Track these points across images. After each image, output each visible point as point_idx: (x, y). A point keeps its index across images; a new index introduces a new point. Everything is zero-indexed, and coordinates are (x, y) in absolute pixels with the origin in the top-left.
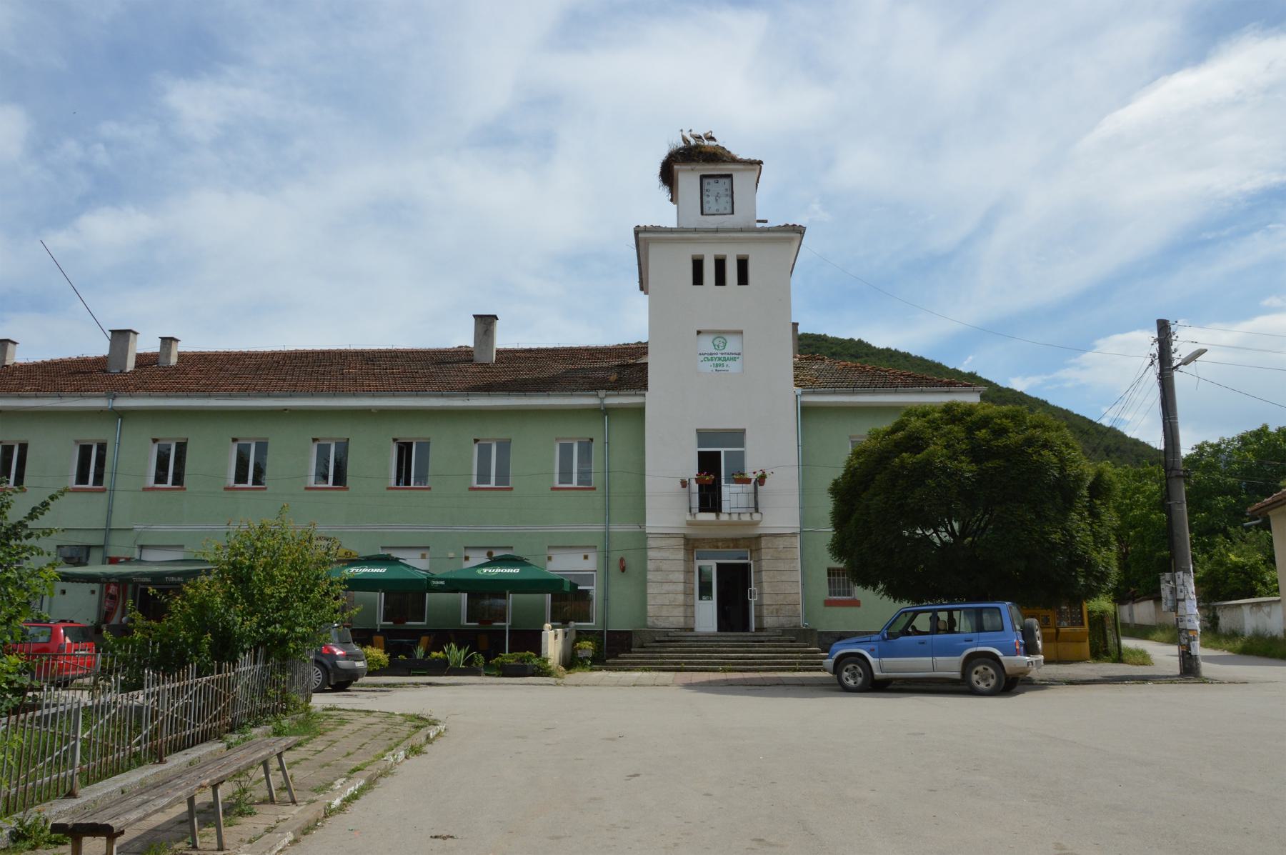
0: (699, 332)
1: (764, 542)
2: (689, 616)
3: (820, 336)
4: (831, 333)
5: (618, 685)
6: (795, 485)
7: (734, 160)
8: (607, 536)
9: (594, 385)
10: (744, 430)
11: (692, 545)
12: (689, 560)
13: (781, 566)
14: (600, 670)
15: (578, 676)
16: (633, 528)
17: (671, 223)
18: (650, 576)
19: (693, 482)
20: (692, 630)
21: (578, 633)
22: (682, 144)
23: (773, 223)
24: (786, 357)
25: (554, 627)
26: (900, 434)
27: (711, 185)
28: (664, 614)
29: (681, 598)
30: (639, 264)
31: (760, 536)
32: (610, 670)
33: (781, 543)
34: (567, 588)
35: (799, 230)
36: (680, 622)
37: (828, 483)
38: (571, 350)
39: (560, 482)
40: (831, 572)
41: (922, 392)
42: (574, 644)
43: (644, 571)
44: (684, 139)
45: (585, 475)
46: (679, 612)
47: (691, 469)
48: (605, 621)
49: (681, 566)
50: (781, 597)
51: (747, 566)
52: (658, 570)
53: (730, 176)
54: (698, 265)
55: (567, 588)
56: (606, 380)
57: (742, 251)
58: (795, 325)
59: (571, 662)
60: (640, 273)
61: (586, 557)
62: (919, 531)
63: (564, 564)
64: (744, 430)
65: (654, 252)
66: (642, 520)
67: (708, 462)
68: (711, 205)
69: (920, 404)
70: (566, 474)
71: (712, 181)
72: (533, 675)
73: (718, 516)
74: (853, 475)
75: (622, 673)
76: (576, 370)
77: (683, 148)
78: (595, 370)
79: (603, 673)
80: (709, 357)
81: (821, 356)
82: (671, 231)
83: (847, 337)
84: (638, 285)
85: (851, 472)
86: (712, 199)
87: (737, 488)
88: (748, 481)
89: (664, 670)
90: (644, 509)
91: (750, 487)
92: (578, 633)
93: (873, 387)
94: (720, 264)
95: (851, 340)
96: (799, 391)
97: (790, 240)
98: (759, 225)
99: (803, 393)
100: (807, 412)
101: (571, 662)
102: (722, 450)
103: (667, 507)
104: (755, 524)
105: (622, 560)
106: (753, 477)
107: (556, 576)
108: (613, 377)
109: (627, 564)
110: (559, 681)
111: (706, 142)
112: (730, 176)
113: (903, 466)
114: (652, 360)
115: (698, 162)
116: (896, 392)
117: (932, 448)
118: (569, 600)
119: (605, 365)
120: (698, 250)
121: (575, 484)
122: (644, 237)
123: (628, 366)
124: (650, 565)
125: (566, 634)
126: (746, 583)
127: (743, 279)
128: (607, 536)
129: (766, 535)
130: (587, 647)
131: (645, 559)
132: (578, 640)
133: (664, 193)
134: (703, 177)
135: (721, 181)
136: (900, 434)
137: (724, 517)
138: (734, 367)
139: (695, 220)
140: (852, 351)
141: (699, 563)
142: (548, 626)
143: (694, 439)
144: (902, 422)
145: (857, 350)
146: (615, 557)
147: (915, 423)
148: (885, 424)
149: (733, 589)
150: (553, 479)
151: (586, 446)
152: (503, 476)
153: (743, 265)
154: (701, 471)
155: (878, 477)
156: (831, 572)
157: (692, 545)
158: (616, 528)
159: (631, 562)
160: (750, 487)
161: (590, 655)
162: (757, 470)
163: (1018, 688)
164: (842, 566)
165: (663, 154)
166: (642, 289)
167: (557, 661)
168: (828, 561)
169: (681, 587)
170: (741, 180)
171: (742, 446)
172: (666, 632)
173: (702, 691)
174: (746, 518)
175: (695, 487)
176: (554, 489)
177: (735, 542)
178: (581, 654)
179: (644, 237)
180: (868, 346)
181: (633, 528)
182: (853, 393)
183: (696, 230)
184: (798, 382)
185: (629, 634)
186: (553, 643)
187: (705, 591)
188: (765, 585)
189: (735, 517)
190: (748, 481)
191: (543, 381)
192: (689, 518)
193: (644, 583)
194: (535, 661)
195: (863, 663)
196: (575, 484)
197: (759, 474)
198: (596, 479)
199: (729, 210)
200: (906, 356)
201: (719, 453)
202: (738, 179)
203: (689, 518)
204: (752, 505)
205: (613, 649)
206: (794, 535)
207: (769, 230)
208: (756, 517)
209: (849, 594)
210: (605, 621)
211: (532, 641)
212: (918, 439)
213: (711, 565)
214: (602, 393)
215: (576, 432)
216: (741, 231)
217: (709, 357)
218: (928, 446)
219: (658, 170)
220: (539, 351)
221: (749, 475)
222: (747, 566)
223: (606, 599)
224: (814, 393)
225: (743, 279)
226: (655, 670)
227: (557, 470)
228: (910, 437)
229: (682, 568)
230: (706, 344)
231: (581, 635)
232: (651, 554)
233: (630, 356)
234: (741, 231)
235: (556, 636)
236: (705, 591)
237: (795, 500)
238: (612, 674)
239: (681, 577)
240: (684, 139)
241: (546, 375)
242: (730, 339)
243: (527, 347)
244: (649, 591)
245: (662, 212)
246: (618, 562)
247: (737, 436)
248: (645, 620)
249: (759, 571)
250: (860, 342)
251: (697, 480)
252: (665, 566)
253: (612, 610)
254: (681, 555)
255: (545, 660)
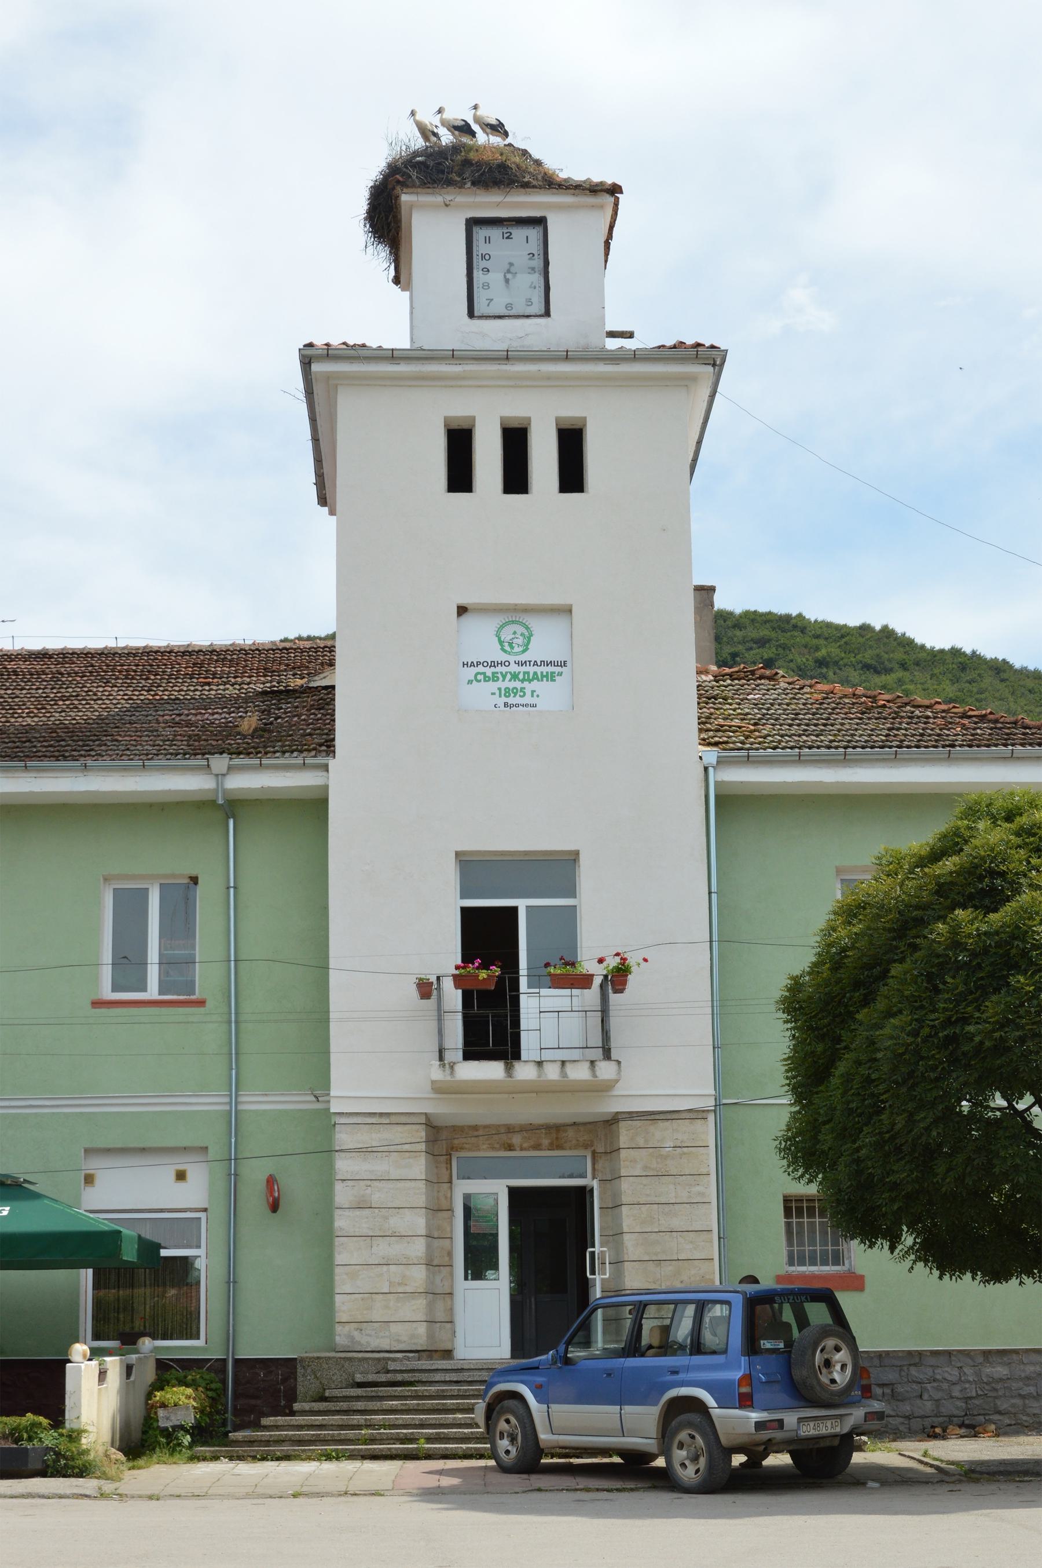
0: (462, 610)
1: (625, 1134)
2: (443, 1319)
3: (787, 618)
4: (816, 611)
5: (257, 1494)
6: (701, 990)
7: (551, 183)
8: (234, 1122)
9: (200, 743)
10: (577, 853)
11: (446, 1142)
12: (439, 1182)
13: (669, 1191)
14: (215, 1458)
15: (160, 1473)
16: (300, 1102)
17: (400, 340)
18: (342, 1222)
19: (448, 984)
20: (448, 1354)
21: (162, 1365)
22: (419, 143)
23: (644, 340)
24: (677, 668)
25: (95, 1353)
26: (949, 864)
27: (493, 244)
28: (378, 1314)
29: (418, 1275)
30: (316, 440)
31: (613, 1121)
32: (241, 1458)
33: (665, 1134)
34: (129, 1254)
35: (712, 358)
36: (418, 1336)
37: (777, 987)
38: (148, 654)
39: (115, 988)
40: (792, 1206)
41: (1012, 758)
42: (149, 1395)
43: (325, 1209)
44: (425, 132)
45: (177, 967)
46: (415, 1309)
47: (444, 952)
48: (230, 1337)
49: (418, 1194)
50: (668, 1269)
51: (583, 1194)
52: (362, 1205)
53: (540, 222)
54: (460, 443)
55: (129, 1254)
56: (230, 730)
57: (570, 407)
58: (705, 592)
59: (142, 1439)
60: (318, 461)
61: (181, 1176)
62: (999, 1101)
63: (125, 1194)
64: (577, 853)
65: (352, 411)
66: (319, 1080)
67: (487, 936)
68: (493, 292)
69: (999, 787)
70: (129, 964)
71: (495, 233)
72: (43, 1474)
73: (509, 1069)
74: (837, 966)
75: (270, 1466)
76: (156, 705)
77: (424, 152)
78: (205, 704)
79: (222, 1467)
80: (486, 670)
81: (769, 669)
82: (393, 356)
83: (854, 622)
84: (313, 491)
85: (833, 960)
86: (495, 278)
87: (557, 998)
88: (584, 981)
89: (375, 1457)
90: (327, 1052)
91: (591, 996)
92: (162, 1365)
93: (893, 746)
94: (515, 441)
95: (865, 628)
96: (711, 755)
97: (686, 382)
98: (612, 344)
99: (721, 762)
100: (729, 807)
101: (142, 1439)
102: (522, 904)
103: (387, 1050)
104: (605, 1088)
105: (271, 1181)
106: (598, 972)
107: (102, 1223)
108: (250, 722)
109: (283, 1192)
110: (108, 1487)
111: (482, 138)
112: (540, 222)
113: (956, 945)
114: (347, 681)
115: (461, 185)
116: (949, 759)
117: (1026, 897)
118: (139, 1286)
119: (231, 691)
120: (459, 406)
121: (153, 991)
122: (326, 372)
123: (289, 693)
124: (342, 1194)
125: (129, 1370)
126: (583, 1238)
127: (572, 477)
128: (234, 1122)
129: (632, 1116)
130: (183, 1403)
131: (327, 1180)
132: (160, 1384)
133: (377, 261)
134: (472, 223)
135: (519, 233)
136: (949, 864)
137: (524, 1072)
138: (549, 696)
139: (455, 330)
140: (868, 656)
141: (463, 1187)
142: (79, 1350)
143: (450, 875)
144: (957, 832)
145: (879, 652)
146: (255, 1174)
147: (990, 836)
148: (917, 838)
149: (550, 1244)
150: (96, 979)
151: (182, 895)
152: (177, 967)
153: (571, 442)
154: (467, 956)
155: (896, 970)
156: (792, 1206)
157: (446, 1142)
158: (255, 1102)
159: (296, 1187)
160: (591, 996)
161: (189, 1419)
162: (608, 953)
163: (304, 1418)
164: (813, 1189)
165: (373, 170)
166: (323, 500)
167: (106, 1436)
168: (780, 1180)
169: (418, 1248)
170: (569, 232)
171: (572, 893)
172: (381, 1360)
173: (462, 1506)
174: (579, 1073)
175: (453, 998)
176: (98, 1004)
177: (554, 1134)
178: (165, 1419)
179: (326, 372)
180: (907, 643)
181: (300, 1102)
182: (845, 761)
183: (453, 356)
184: (711, 733)
185: (290, 1363)
186: (95, 1394)
187: (479, 1260)
188: (628, 1240)
189: (552, 1073)
190: (584, 981)
191: (71, 731)
192: (437, 1073)
193: (325, 1239)
194: (49, 1438)
195: (521, 1411)
196: (153, 991)
197: (613, 962)
198: (206, 979)
199: (538, 307)
200: (1000, 669)
201: (514, 910)
202: (562, 229)
203: (437, 1073)
204: (596, 1040)
205: (247, 1406)
206: (696, 1114)
207: (635, 356)
208: (606, 1070)
209: (837, 1259)
210: (230, 1337)
211: (43, 1387)
212: (993, 874)
213: (494, 1193)
214: (220, 763)
215: (154, 861)
216: (567, 357)
217: (486, 670)
218: (1017, 891)
219: (361, 205)
220: (66, 656)
221: (588, 965)
222: (583, 1194)
223: (232, 1282)
224: (748, 761)
225: (572, 477)
226: (352, 1456)
227: (107, 956)
228: (973, 871)
229: (421, 1200)
230: (481, 639)
231: (168, 1371)
232: (343, 1165)
233: (296, 669)
234: (567, 357)
235: (102, 1375)
236: (479, 1260)
237: (700, 1027)
238: (247, 1470)
239: (419, 1222)
240: (425, 132)
241: (79, 716)
242: (536, 624)
243: (35, 645)
244: (340, 1258)
245: (374, 311)
246: (262, 1186)
247: (558, 870)
248: (331, 1332)
249: (614, 1207)
250: (887, 633)
251: (458, 980)
252: (378, 1195)
253: (249, 1314)
254: (419, 1167)
255: (74, 1436)
